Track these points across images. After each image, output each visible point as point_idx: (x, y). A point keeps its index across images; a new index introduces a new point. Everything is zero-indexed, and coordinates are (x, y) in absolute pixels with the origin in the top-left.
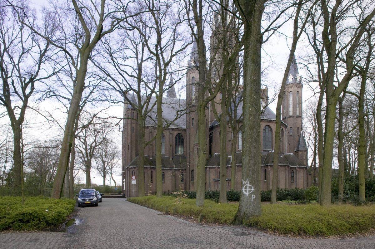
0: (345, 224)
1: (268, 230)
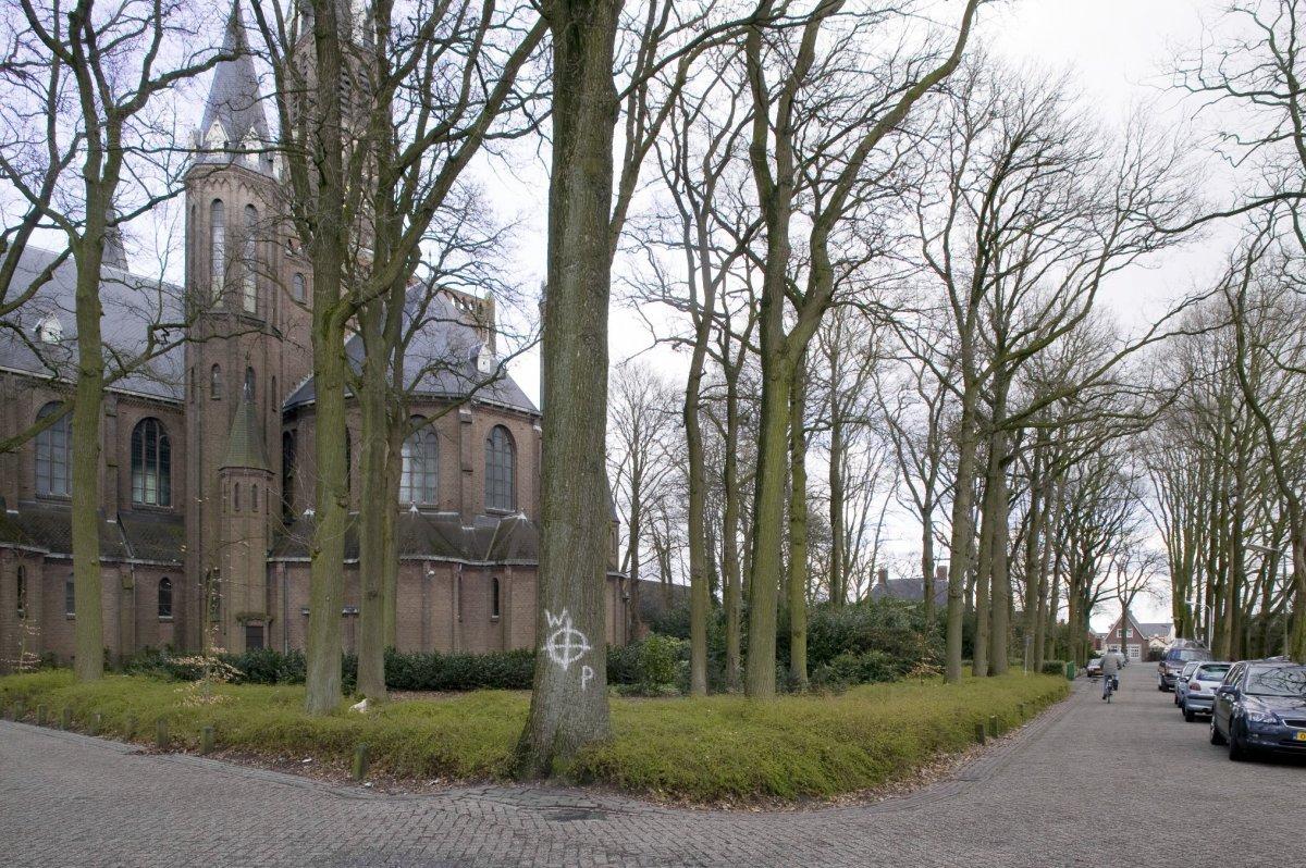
0: (863, 755)
1: (651, 790)
